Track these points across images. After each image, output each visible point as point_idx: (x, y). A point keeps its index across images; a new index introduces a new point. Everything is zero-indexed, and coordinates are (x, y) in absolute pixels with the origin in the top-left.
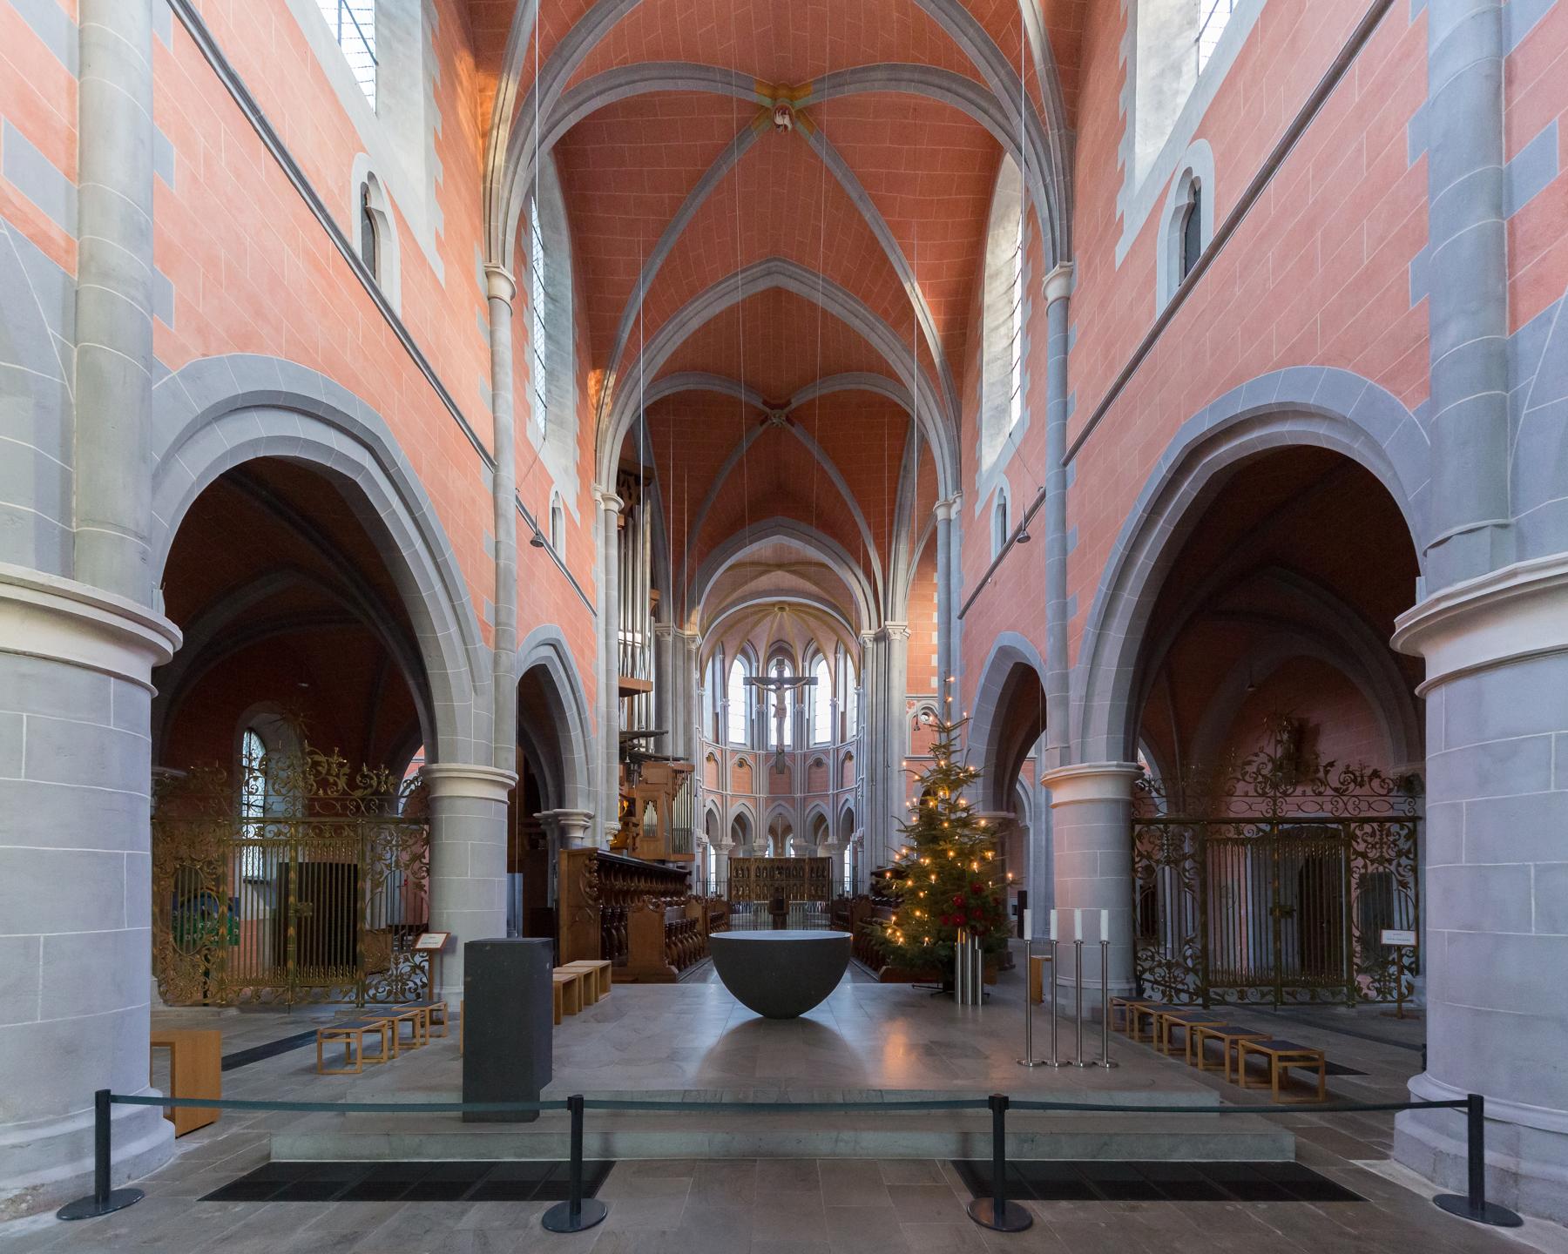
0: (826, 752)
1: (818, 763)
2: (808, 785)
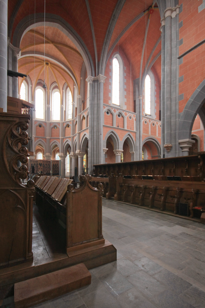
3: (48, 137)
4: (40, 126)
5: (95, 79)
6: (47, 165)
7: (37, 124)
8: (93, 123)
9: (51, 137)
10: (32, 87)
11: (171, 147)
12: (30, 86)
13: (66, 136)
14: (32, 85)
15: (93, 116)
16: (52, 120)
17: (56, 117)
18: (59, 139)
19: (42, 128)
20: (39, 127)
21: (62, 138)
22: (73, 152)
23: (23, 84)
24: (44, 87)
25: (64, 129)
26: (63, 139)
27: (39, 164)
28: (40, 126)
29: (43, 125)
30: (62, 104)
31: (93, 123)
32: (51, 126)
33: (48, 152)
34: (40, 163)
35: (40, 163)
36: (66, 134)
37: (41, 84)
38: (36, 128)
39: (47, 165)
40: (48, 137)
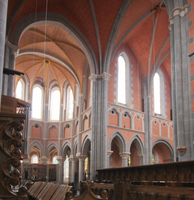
1: (68, 126)
2: (49, 135)
3: (45, 139)
4: (37, 126)
6: (42, 169)
7: (33, 124)
9: (49, 138)
11: (185, 149)
13: (65, 137)
16: (50, 120)
18: (58, 140)
21: (61, 139)
22: (73, 155)
24: (43, 85)
25: (63, 129)
27: (34, 168)
28: (37, 126)
29: (40, 125)
30: (62, 103)
33: (44, 154)
34: (35, 167)
35: (35, 167)
37: (39, 82)
38: (32, 129)
39: (42, 169)
40: (45, 139)
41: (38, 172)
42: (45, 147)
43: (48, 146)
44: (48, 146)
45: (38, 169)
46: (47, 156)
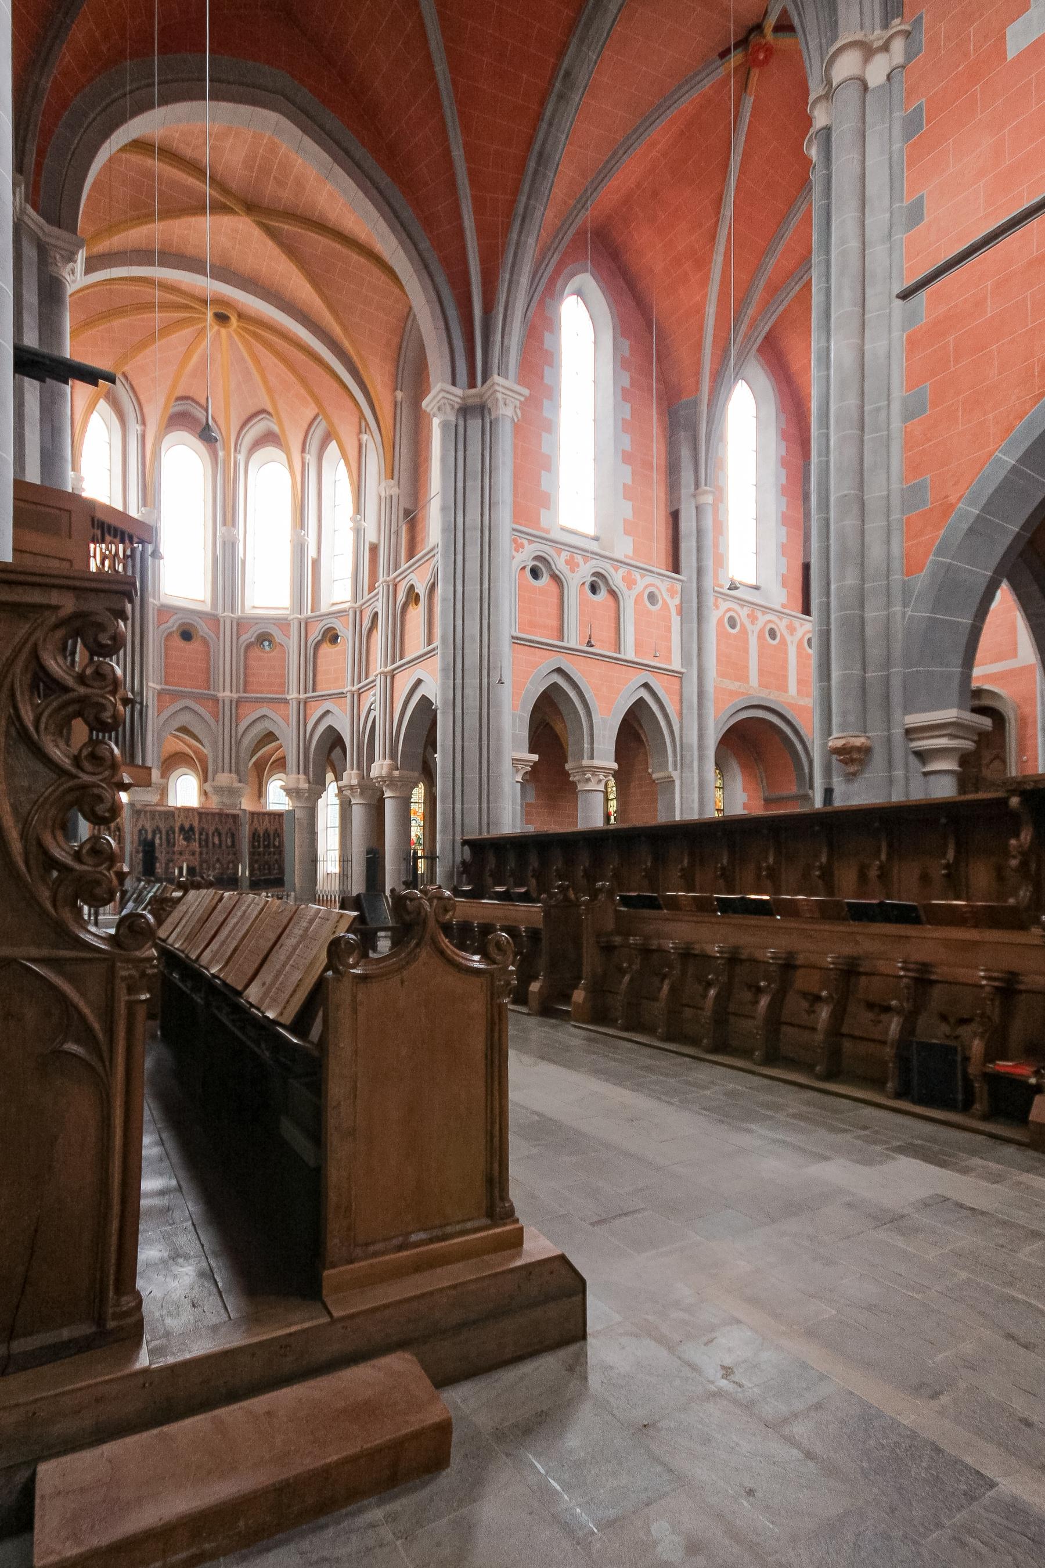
0: (282, 623)
3: (227, 693)
4: (187, 635)
5: (470, 402)
6: (220, 835)
8: (459, 622)
9: (245, 691)
10: (143, 436)
12: (134, 428)
13: (318, 687)
14: (144, 423)
15: (459, 589)
16: (248, 604)
17: (268, 593)
18: (286, 701)
19: (195, 645)
20: (178, 642)
21: (302, 696)
22: (355, 771)
23: (95, 419)
24: (206, 435)
26: (305, 703)
29: (203, 629)
30: (302, 527)
31: (459, 622)
32: (243, 638)
33: (227, 766)
35: (187, 826)
36: (319, 678)
37: (189, 418)
39: (220, 835)
40: (226, 694)
41: (200, 846)
42: (227, 730)
43: (242, 727)
44: (242, 727)
45: (201, 834)
46: (238, 772)
